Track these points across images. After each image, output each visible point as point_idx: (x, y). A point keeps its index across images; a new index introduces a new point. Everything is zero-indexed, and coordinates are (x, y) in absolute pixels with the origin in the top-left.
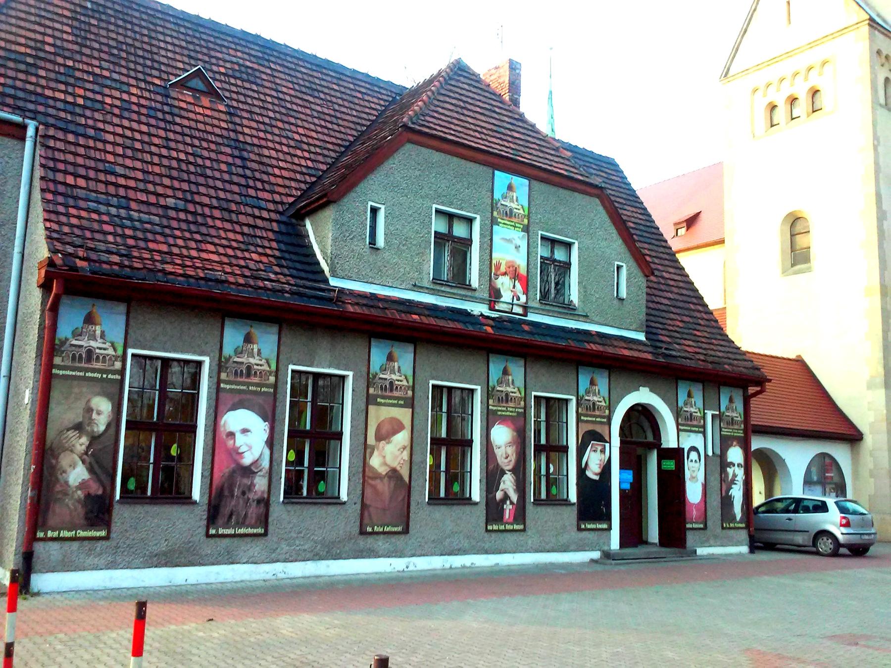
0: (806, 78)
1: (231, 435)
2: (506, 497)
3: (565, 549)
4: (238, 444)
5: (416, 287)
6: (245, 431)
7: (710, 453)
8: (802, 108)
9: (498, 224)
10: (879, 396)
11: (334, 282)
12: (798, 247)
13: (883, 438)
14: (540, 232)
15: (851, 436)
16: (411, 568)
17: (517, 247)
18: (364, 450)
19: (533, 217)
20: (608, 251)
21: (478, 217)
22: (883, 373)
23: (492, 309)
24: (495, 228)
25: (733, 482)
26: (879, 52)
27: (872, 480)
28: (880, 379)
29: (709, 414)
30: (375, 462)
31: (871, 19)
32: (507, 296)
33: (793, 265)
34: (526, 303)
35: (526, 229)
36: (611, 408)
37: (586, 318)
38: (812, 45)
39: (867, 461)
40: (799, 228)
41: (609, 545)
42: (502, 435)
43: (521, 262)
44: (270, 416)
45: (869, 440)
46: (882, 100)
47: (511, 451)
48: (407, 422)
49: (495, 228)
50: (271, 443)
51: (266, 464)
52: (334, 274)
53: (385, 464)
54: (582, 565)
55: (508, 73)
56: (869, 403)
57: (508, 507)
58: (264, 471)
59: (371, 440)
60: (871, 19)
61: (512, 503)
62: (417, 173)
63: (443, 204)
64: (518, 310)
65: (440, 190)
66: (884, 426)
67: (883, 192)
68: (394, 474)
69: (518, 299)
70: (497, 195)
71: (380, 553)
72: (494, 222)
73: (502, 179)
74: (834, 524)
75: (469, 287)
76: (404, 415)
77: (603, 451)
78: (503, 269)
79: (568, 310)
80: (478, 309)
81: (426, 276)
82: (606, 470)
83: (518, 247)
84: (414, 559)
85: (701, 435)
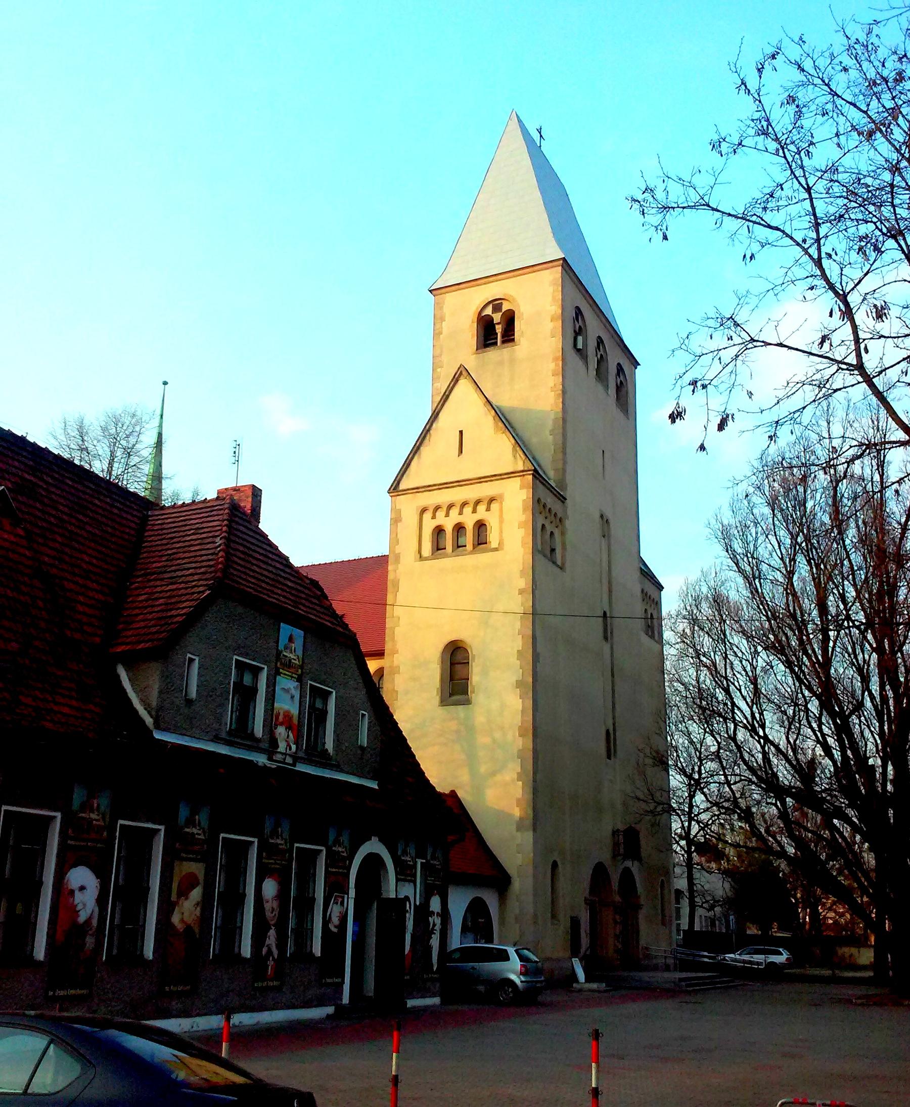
0: (474, 511)
1: (72, 892)
2: (270, 952)
3: (307, 1005)
4: (76, 902)
5: (216, 739)
6: (82, 888)
7: (418, 903)
8: (469, 538)
9: (279, 674)
10: (528, 838)
11: (158, 735)
12: (457, 677)
13: (530, 881)
14: (309, 682)
15: (498, 878)
16: (195, 1029)
17: (292, 697)
18: (166, 907)
19: (307, 667)
20: (356, 700)
21: (266, 667)
22: (532, 816)
23: (270, 759)
24: (278, 678)
25: (432, 932)
26: (539, 501)
27: (517, 926)
28: (529, 822)
29: (419, 861)
30: (176, 919)
31: (535, 470)
32: (282, 747)
33: (451, 695)
34: (296, 753)
35: (299, 679)
36: (351, 858)
37: (338, 768)
38: (481, 480)
39: (513, 906)
40: (459, 657)
41: (341, 1000)
42: (270, 888)
43: (295, 711)
44: (102, 874)
45: (516, 885)
46: (539, 547)
47: (275, 904)
48: (201, 877)
49: (278, 678)
50: (101, 900)
51: (95, 922)
52: (157, 726)
53: (182, 921)
54: (321, 1021)
55: (250, 499)
56: (517, 845)
57: (271, 963)
58: (94, 930)
59: (174, 897)
60: (535, 470)
61: (273, 958)
62: (224, 625)
63: (246, 655)
64: (289, 760)
65: (239, 642)
66: (530, 870)
67: (538, 634)
68: (188, 928)
69: (290, 749)
70: (281, 647)
71: (174, 1012)
72: (278, 673)
73: (286, 630)
74: (515, 973)
75: (252, 736)
76: (197, 869)
77: (342, 904)
78: (281, 718)
79: (323, 759)
80: (261, 759)
81: (223, 727)
82: (344, 918)
83: (292, 697)
84: (198, 1019)
85: (412, 884)
